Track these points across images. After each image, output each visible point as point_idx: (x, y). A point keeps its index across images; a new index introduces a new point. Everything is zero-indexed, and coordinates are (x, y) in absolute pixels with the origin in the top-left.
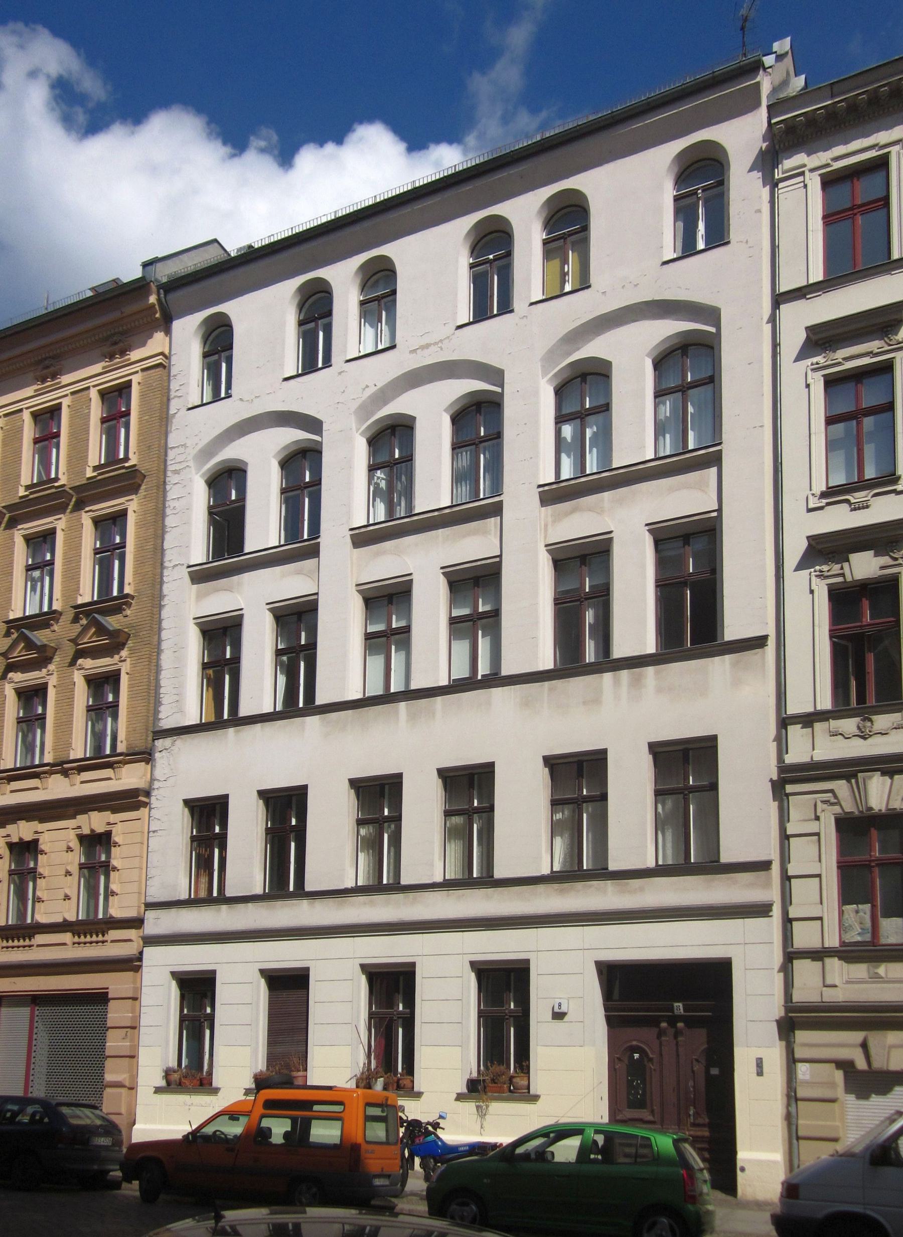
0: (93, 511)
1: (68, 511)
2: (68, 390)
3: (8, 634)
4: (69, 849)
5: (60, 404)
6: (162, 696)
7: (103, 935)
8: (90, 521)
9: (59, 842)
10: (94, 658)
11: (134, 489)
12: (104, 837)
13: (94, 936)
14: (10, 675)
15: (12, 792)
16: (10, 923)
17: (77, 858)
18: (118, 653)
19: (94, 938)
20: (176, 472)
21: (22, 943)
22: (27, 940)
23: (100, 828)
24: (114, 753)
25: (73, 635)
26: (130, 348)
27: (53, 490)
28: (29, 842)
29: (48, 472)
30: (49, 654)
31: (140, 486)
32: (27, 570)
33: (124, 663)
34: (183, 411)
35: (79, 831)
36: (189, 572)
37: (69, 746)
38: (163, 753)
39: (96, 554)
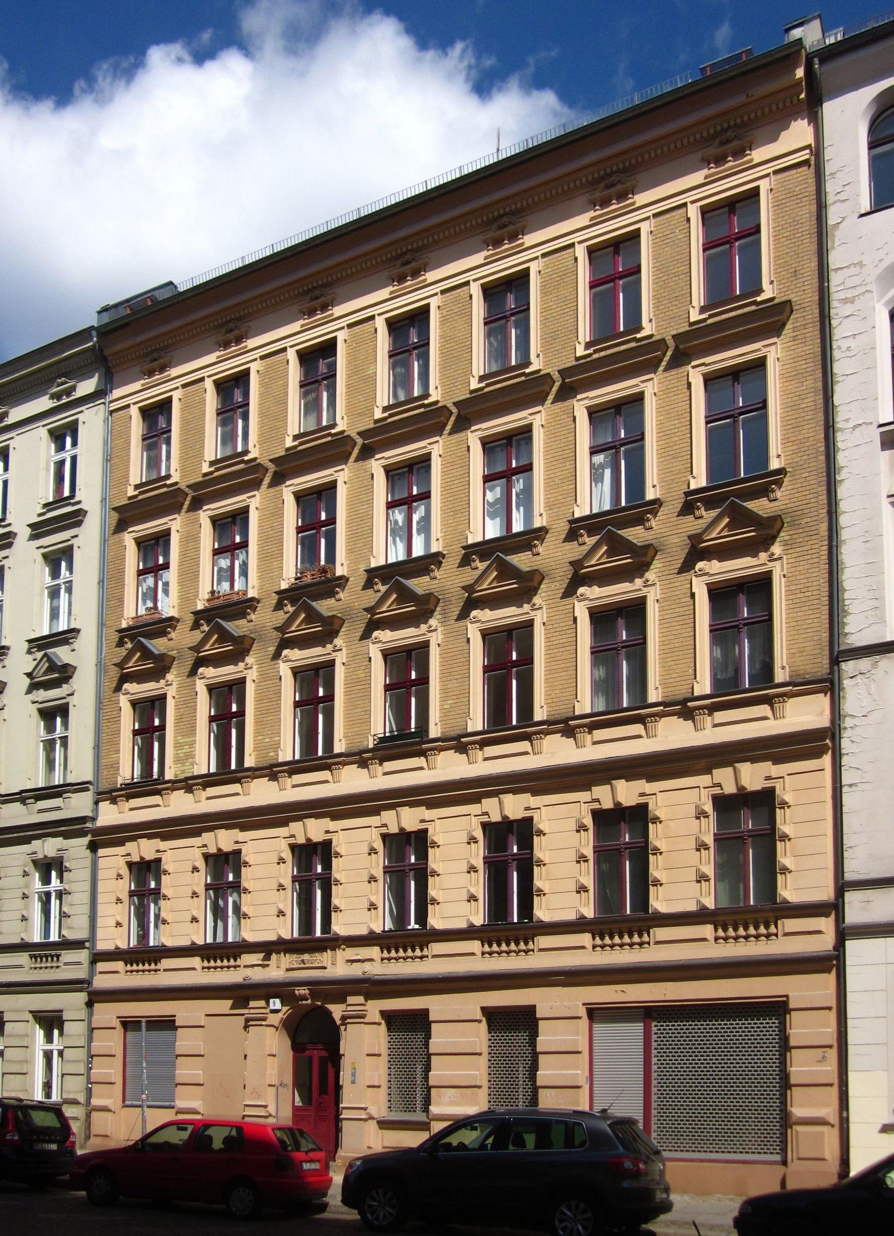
0: (387, 458)
1: (661, 368)
2: (179, 383)
3: (120, 643)
4: (195, 869)
5: (171, 397)
6: (846, 603)
7: (156, 964)
8: (292, 497)
9: (182, 862)
10: (139, 682)
11: (776, 329)
12: (153, 865)
13: (147, 965)
14: (285, 652)
15: (208, 798)
16: (230, 940)
17: (201, 879)
18: (164, 678)
19: (147, 967)
20: (850, 301)
21: (141, 967)
22: (153, 964)
23: (149, 856)
24: (161, 780)
25: (117, 660)
26: (333, 303)
27: (165, 490)
28: (150, 862)
29: (409, 389)
30: (247, 646)
31: (784, 325)
32: (139, 575)
33: (781, 564)
34: (853, 219)
35: (205, 850)
36: (881, 433)
37: (276, 746)
38: (859, 679)
39: (298, 533)
